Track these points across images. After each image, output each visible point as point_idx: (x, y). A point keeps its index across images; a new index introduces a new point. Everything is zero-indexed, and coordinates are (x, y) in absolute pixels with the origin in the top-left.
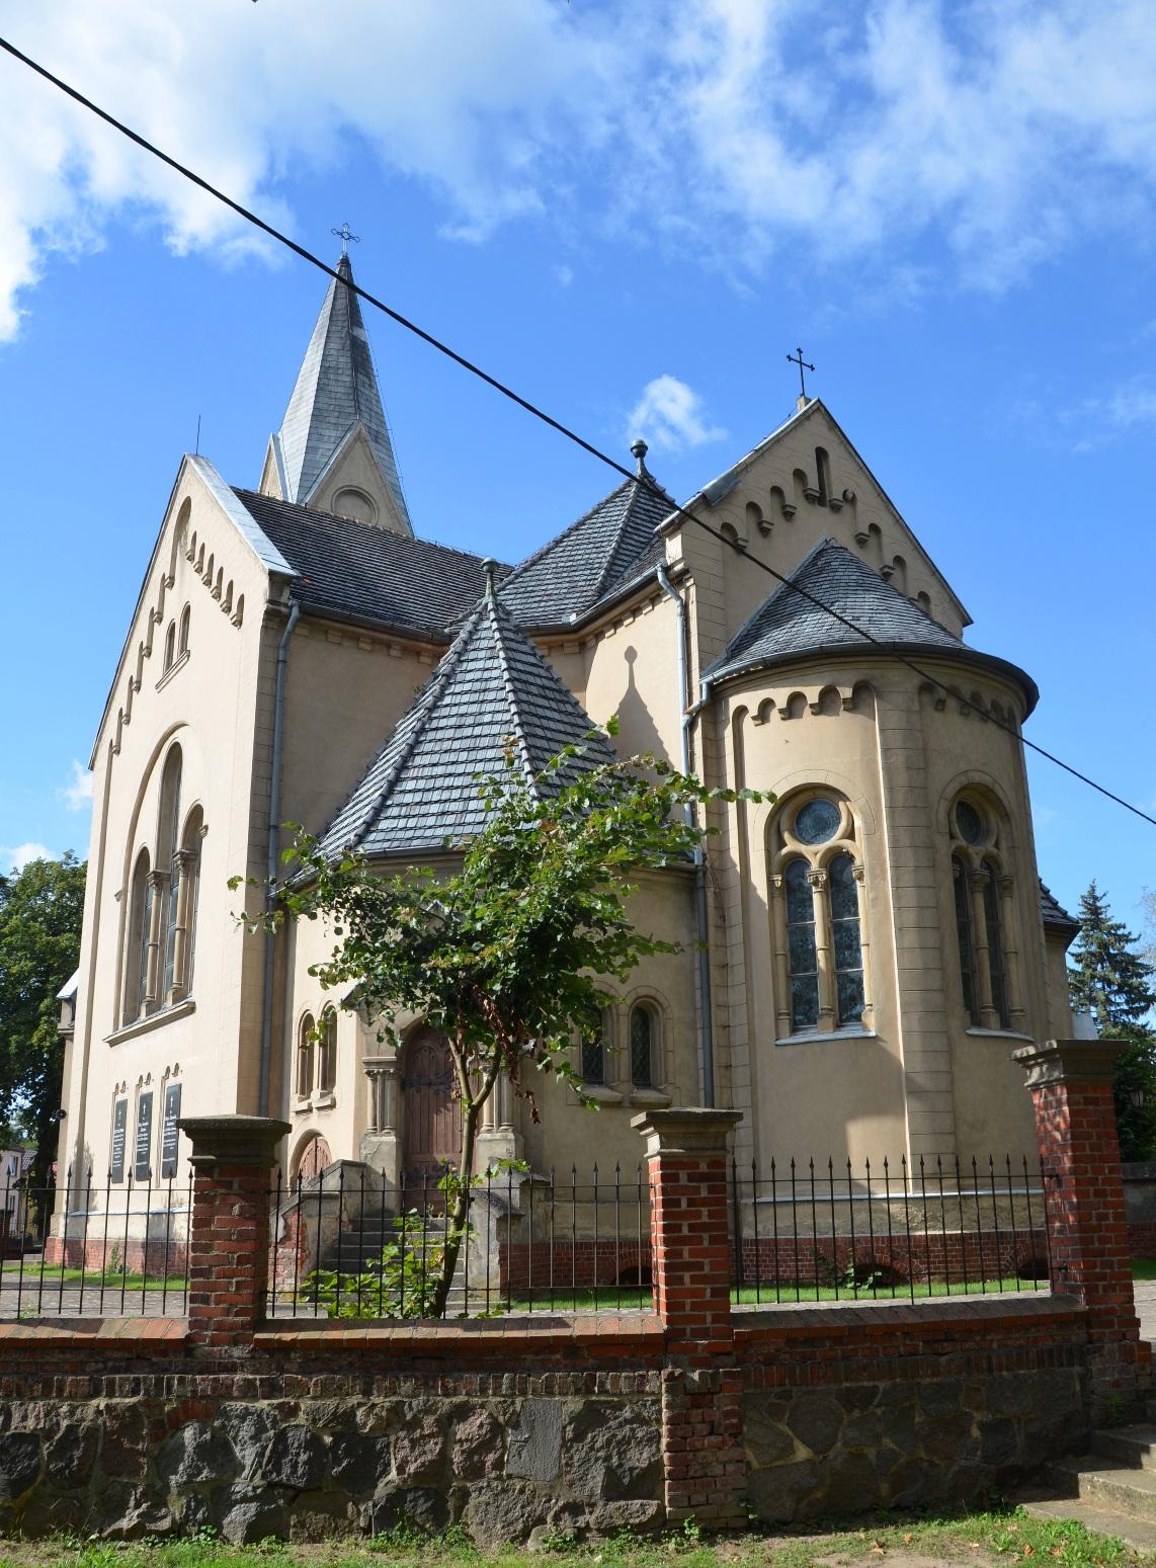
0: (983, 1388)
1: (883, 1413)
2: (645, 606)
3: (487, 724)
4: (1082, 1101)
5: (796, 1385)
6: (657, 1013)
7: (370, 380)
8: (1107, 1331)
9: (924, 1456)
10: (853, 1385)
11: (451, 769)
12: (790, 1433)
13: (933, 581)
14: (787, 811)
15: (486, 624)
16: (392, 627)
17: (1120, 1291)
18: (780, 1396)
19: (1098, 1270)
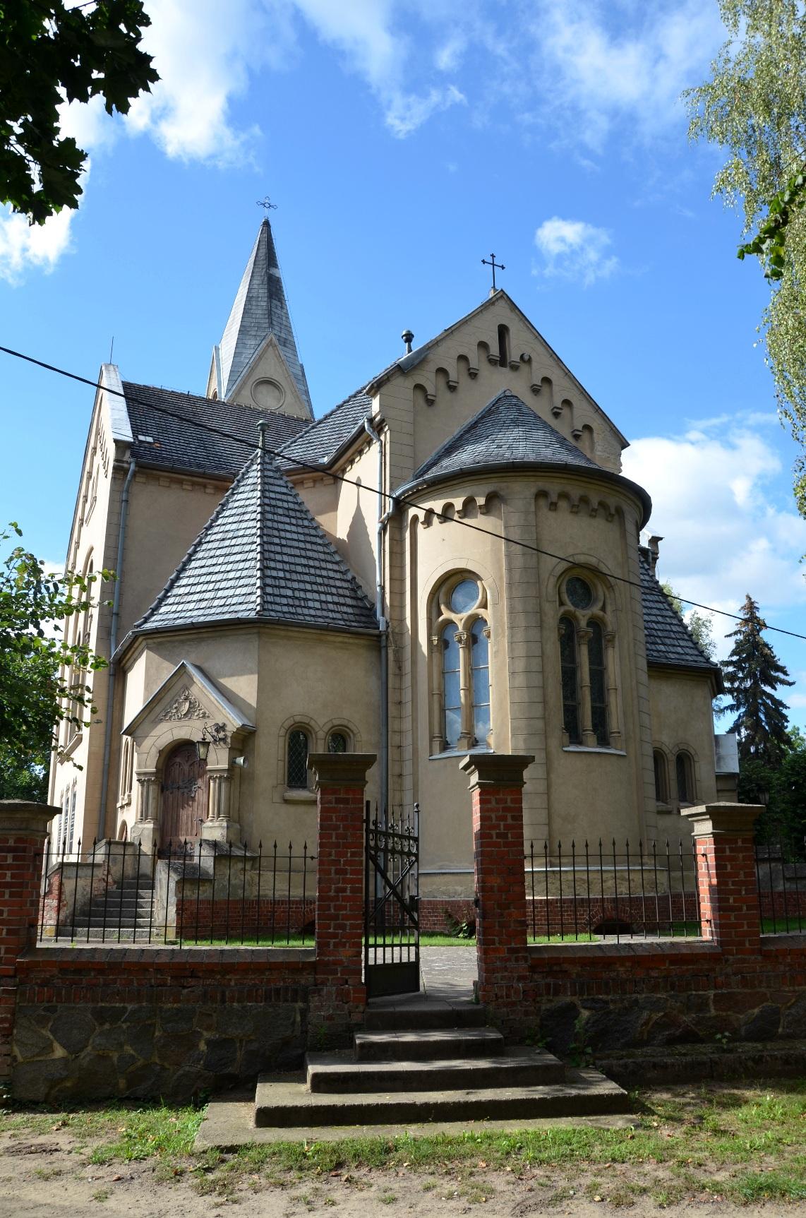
0: (215, 1015)
1: (128, 1027)
2: (365, 447)
3: (241, 536)
4: (334, 800)
5: (61, 1002)
6: (350, 737)
7: (282, 303)
8: (330, 977)
9: (157, 1061)
10: (107, 1005)
11: (211, 569)
12: (51, 1037)
13: (596, 416)
14: (444, 589)
15: (255, 467)
16: (204, 473)
17: (350, 947)
18: (46, 1009)
19: (331, 931)
